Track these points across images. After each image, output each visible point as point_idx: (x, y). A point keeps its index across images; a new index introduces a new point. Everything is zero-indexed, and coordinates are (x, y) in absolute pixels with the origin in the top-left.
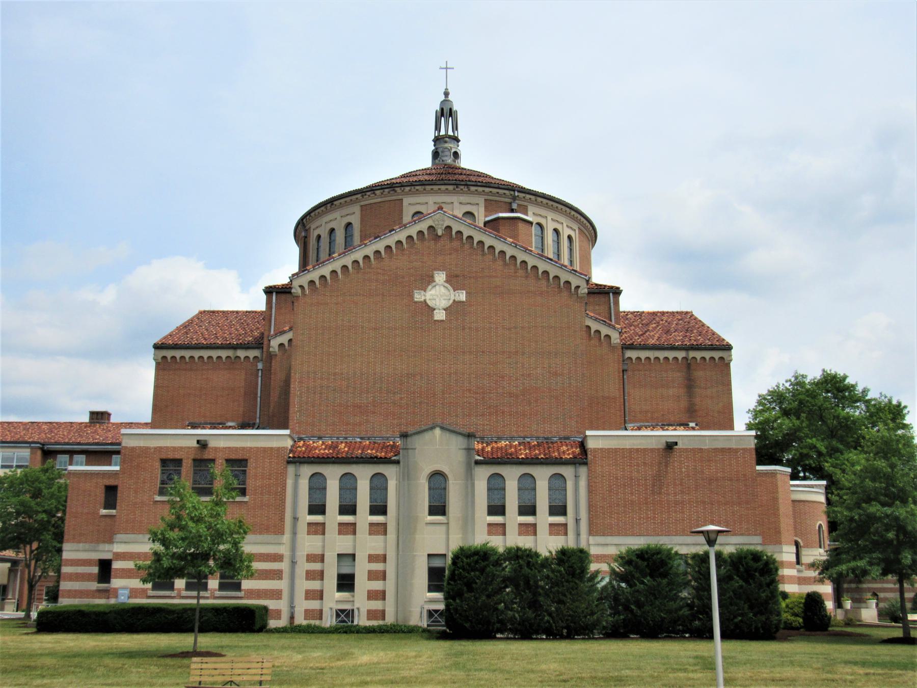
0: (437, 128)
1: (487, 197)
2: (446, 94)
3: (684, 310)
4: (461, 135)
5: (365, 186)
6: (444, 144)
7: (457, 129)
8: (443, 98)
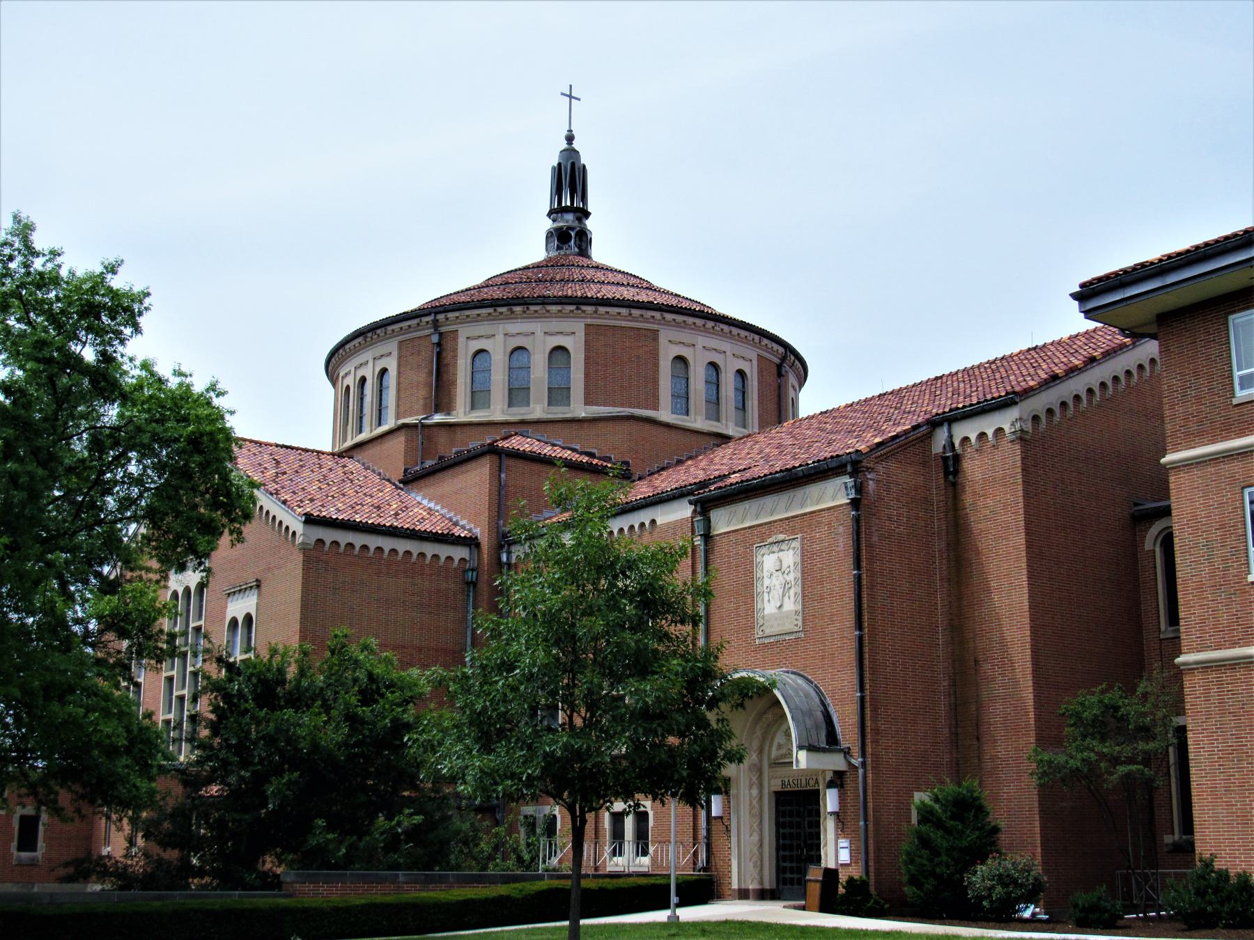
1: (589, 321)
2: (570, 139)
5: (740, 319)
6: (570, 234)
8: (564, 145)
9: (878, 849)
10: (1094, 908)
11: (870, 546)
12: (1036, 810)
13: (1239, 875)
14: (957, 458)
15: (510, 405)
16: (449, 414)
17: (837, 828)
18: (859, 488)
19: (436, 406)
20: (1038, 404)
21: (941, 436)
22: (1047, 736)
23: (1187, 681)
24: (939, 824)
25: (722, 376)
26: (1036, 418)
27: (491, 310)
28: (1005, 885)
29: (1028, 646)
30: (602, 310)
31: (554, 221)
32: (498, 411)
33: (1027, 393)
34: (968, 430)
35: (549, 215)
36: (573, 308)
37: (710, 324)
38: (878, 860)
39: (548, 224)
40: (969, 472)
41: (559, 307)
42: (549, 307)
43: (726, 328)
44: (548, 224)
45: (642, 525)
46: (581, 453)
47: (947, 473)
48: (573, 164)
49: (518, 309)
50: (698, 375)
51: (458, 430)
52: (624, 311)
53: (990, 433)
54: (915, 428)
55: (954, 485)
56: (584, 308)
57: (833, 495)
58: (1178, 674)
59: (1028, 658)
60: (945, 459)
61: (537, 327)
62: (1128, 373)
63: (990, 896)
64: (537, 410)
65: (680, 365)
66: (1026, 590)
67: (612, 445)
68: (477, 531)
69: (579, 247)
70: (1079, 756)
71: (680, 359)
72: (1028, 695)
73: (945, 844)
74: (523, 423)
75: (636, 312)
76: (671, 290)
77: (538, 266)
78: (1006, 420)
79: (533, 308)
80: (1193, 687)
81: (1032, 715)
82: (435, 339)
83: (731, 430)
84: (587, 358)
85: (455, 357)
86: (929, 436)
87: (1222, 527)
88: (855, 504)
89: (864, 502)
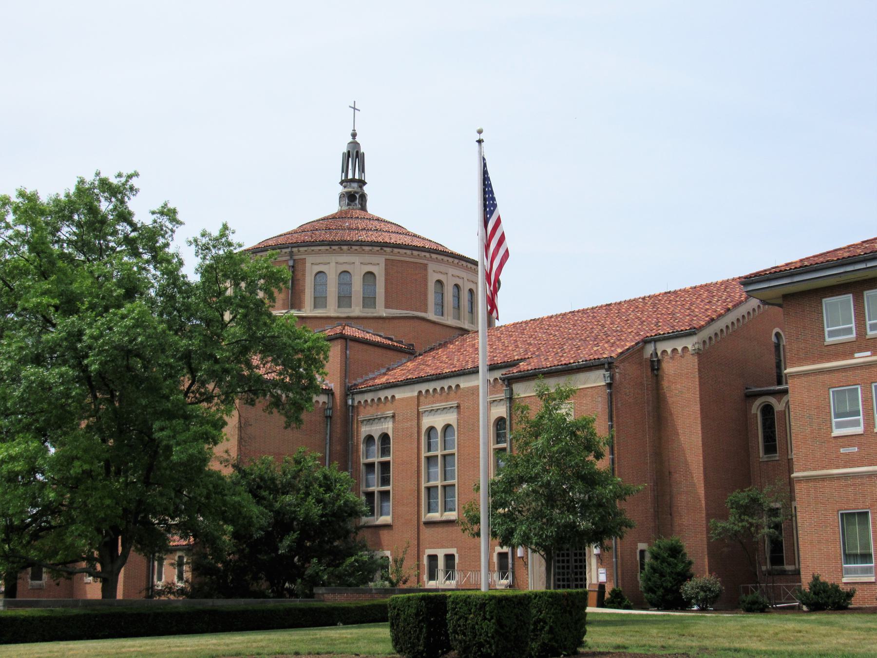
0: (345, 170)
1: (388, 257)
2: (354, 135)
3: (498, 201)
4: (368, 178)
6: (354, 196)
7: (363, 171)
8: (350, 139)
9: (623, 574)
10: (754, 603)
11: (617, 409)
12: (706, 553)
13: (832, 585)
14: (659, 361)
15: (339, 307)
16: (299, 310)
17: (597, 562)
18: (612, 377)
19: (292, 305)
20: (705, 334)
21: (650, 349)
22: (715, 511)
23: (797, 487)
24: (663, 561)
25: (462, 293)
26: (704, 342)
27: (328, 248)
28: (705, 592)
29: (701, 465)
30: (396, 250)
31: (345, 187)
32: (331, 310)
33: (701, 328)
34: (661, 347)
35: (341, 183)
36: (379, 248)
37: (456, 261)
38: (623, 580)
39: (340, 189)
40: (666, 370)
41: (370, 248)
42: (364, 248)
43: (464, 263)
44: (340, 189)
45: (450, 387)
46: (386, 338)
47: (653, 369)
48: (357, 152)
49: (345, 248)
50: (449, 291)
51: (308, 321)
52: (409, 252)
53: (680, 349)
54: (637, 344)
55: (657, 376)
56: (385, 249)
57: (597, 380)
58: (791, 482)
59: (702, 472)
60: (652, 362)
61: (356, 259)
62: (743, 316)
63: (697, 597)
64: (357, 310)
65: (439, 286)
66: (700, 435)
67: (404, 334)
68: (332, 386)
69: (361, 205)
70: (740, 524)
71: (439, 282)
72: (701, 491)
73: (668, 571)
74: (348, 318)
75: (415, 253)
76: (418, 234)
77: (333, 217)
78: (690, 343)
79: (354, 247)
80: (800, 490)
81: (703, 502)
82: (291, 263)
83: (466, 326)
84: (386, 280)
85: (304, 275)
86: (643, 348)
87: (818, 408)
88: (609, 385)
89: (614, 385)
